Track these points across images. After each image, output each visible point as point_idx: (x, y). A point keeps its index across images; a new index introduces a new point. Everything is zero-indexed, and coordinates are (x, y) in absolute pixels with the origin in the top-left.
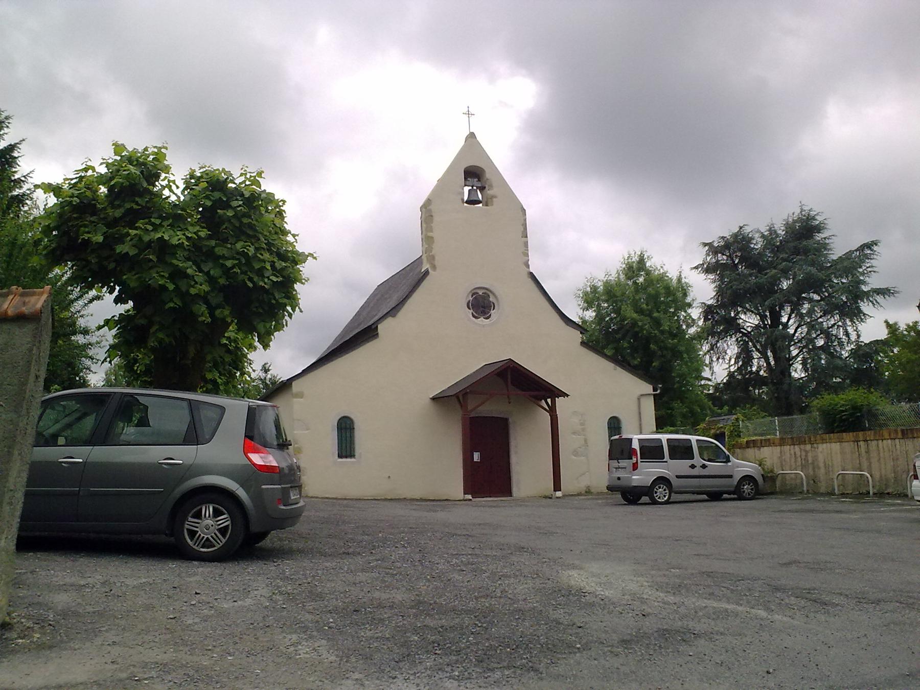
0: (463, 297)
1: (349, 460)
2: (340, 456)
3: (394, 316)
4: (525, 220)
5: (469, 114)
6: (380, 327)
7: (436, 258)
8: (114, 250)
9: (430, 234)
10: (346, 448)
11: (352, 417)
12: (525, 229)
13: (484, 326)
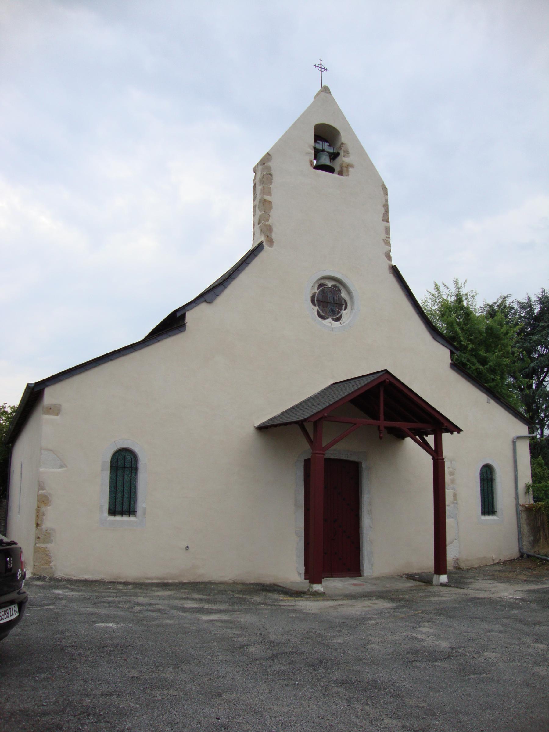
0: (309, 289)
1: (125, 518)
2: (113, 512)
3: (210, 302)
4: (387, 201)
5: (321, 68)
6: (189, 316)
7: (275, 229)
8: (449, 578)
9: (267, 197)
10: (123, 497)
11: (136, 450)
12: (387, 211)
13: (333, 329)
